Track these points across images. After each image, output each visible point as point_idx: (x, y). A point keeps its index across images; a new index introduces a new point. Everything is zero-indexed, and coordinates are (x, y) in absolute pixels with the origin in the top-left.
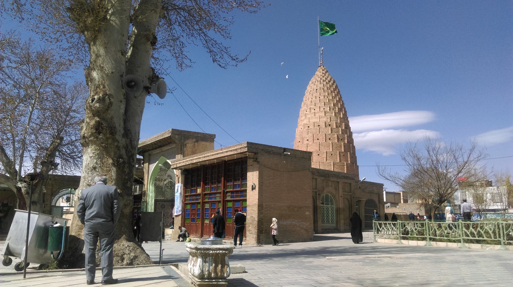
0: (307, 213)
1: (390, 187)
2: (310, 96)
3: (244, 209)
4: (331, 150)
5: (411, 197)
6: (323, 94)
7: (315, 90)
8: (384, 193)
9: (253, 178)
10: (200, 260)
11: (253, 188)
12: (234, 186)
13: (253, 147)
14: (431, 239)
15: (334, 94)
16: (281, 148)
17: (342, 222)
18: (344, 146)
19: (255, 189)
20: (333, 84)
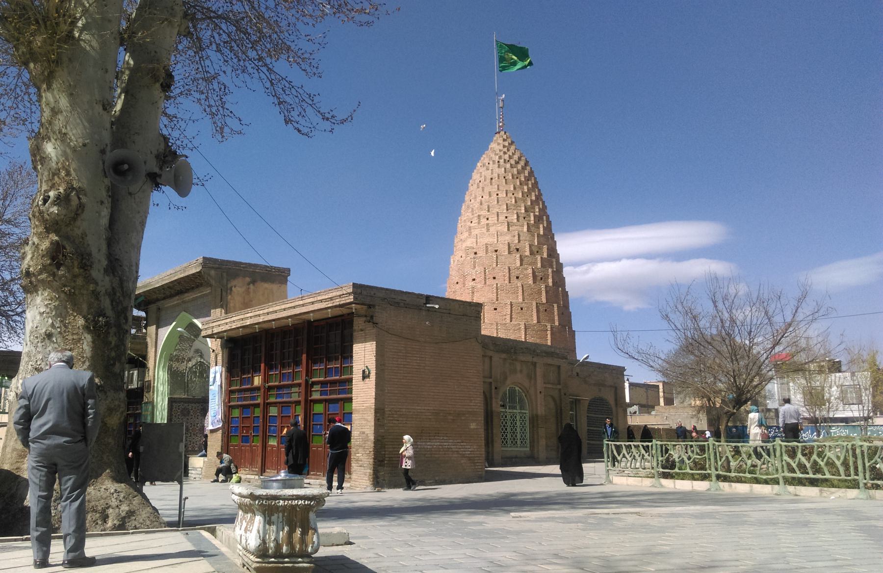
0: (473, 426)
1: (637, 373)
2: (479, 192)
3: (347, 417)
4: (521, 300)
5: (679, 393)
6: (504, 187)
7: (488, 181)
8: (627, 385)
9: (364, 354)
10: (258, 519)
11: (365, 376)
12: (328, 372)
13: (364, 293)
14: (718, 477)
15: (525, 187)
16: (420, 296)
17: (543, 442)
18: (547, 292)
19: (368, 376)
20: (524, 168)
